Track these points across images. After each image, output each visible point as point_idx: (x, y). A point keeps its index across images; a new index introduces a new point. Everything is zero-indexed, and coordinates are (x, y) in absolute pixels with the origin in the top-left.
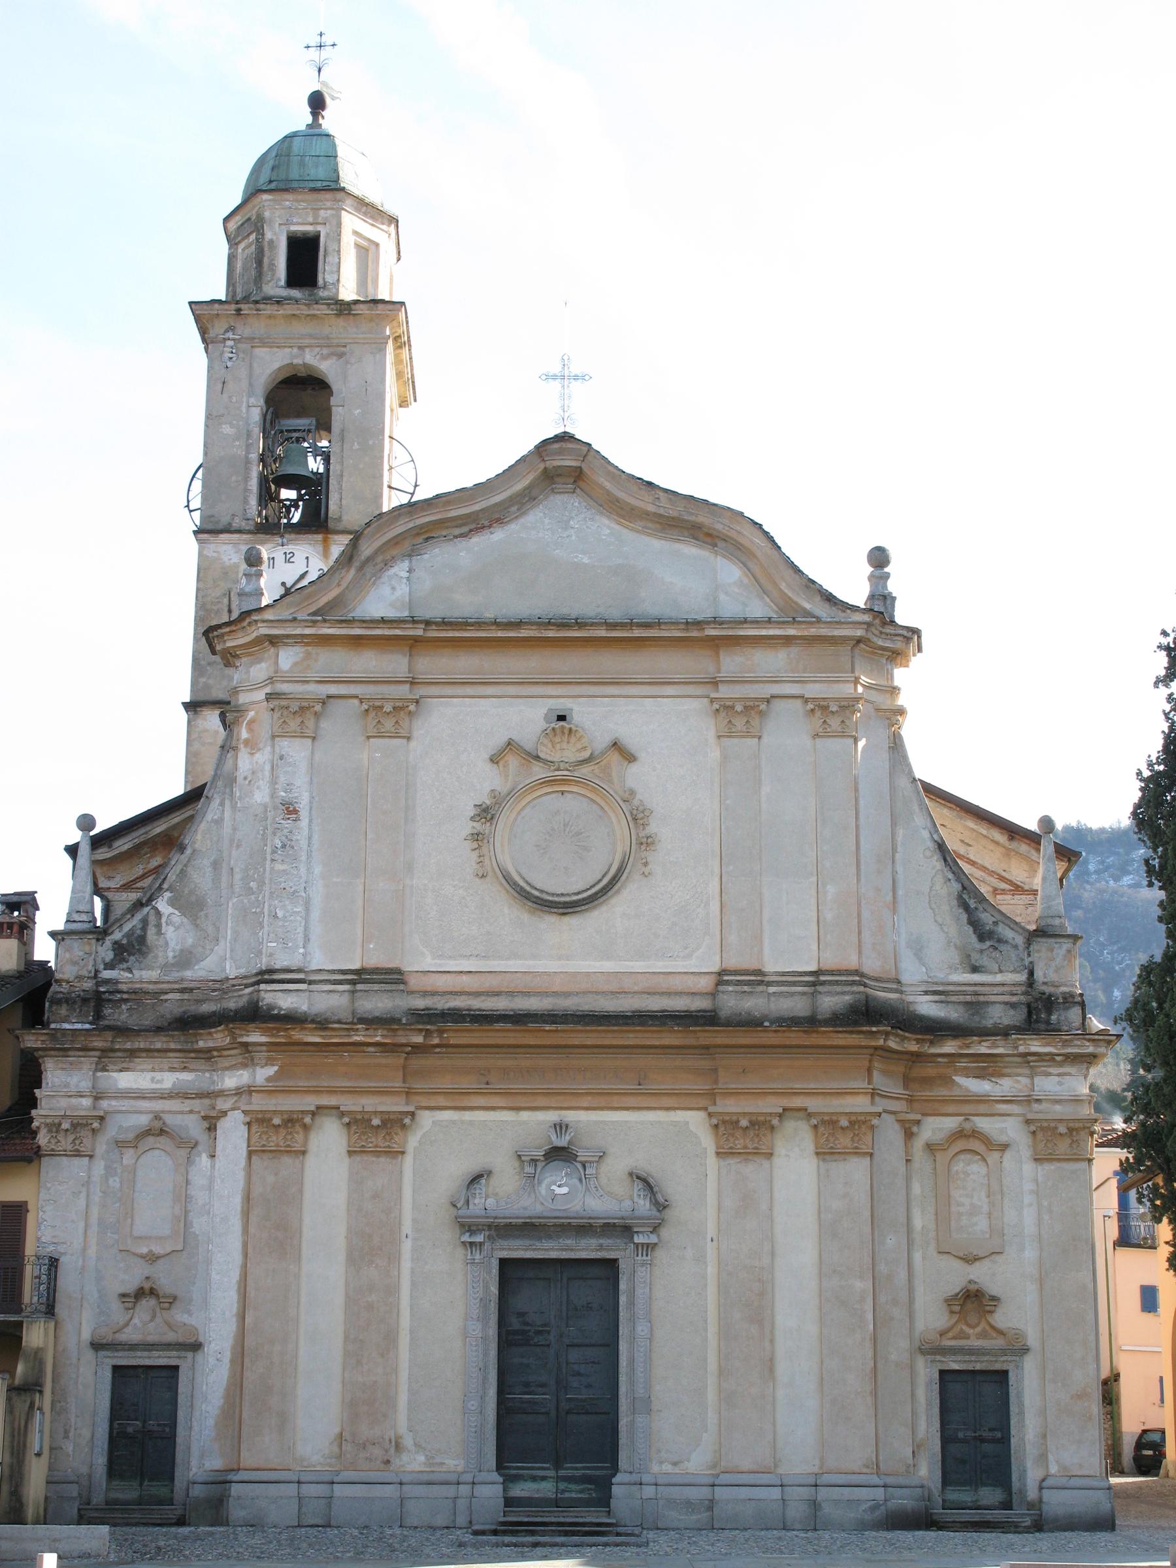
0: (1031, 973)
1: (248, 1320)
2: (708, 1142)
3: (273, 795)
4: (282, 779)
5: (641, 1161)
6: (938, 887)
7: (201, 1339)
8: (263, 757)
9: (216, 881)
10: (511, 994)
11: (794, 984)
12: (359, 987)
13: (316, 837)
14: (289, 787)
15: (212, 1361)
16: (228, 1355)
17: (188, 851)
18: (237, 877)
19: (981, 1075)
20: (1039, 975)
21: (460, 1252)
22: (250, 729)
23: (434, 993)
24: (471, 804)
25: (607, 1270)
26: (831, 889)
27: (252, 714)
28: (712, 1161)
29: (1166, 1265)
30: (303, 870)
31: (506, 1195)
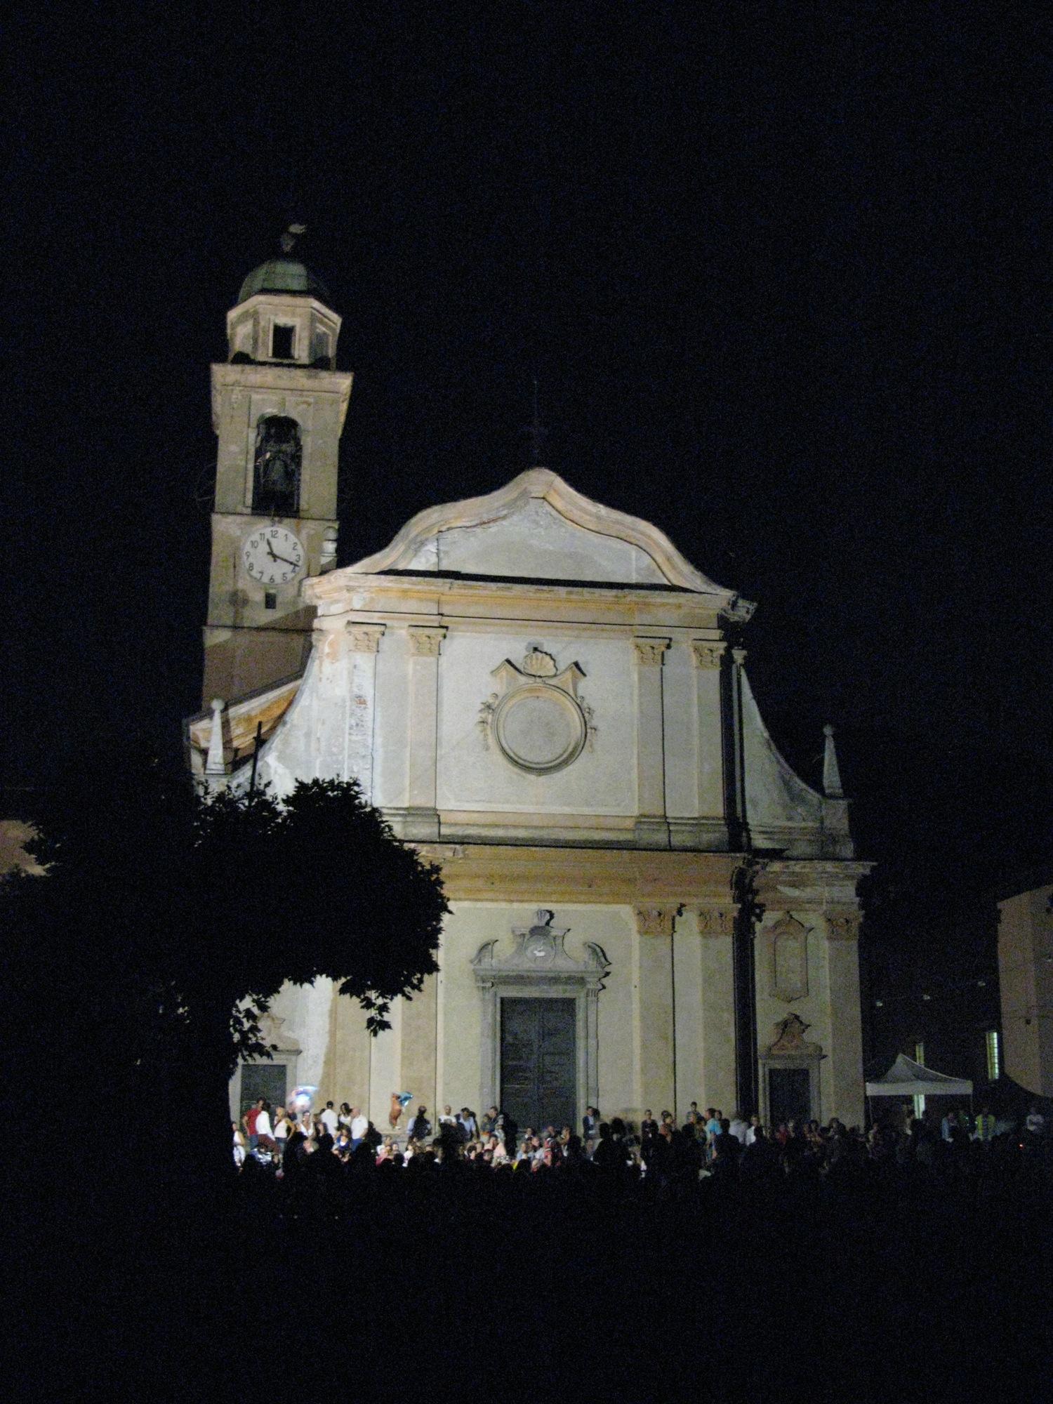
0: (822, 823)
1: (339, 1036)
2: (633, 924)
3: (351, 691)
4: (356, 680)
5: (598, 937)
6: (767, 767)
7: (301, 1048)
8: (343, 665)
9: (308, 745)
10: (505, 826)
11: (685, 824)
12: (409, 819)
13: (378, 719)
14: (360, 687)
15: (310, 1062)
16: (322, 1059)
17: (288, 726)
18: (323, 744)
19: (793, 885)
20: (827, 823)
21: (475, 992)
22: (331, 645)
23: (456, 824)
24: (479, 701)
25: (568, 1006)
26: (707, 766)
27: (332, 637)
28: (636, 939)
29: (307, 986)
30: (370, 740)
31: (505, 955)
